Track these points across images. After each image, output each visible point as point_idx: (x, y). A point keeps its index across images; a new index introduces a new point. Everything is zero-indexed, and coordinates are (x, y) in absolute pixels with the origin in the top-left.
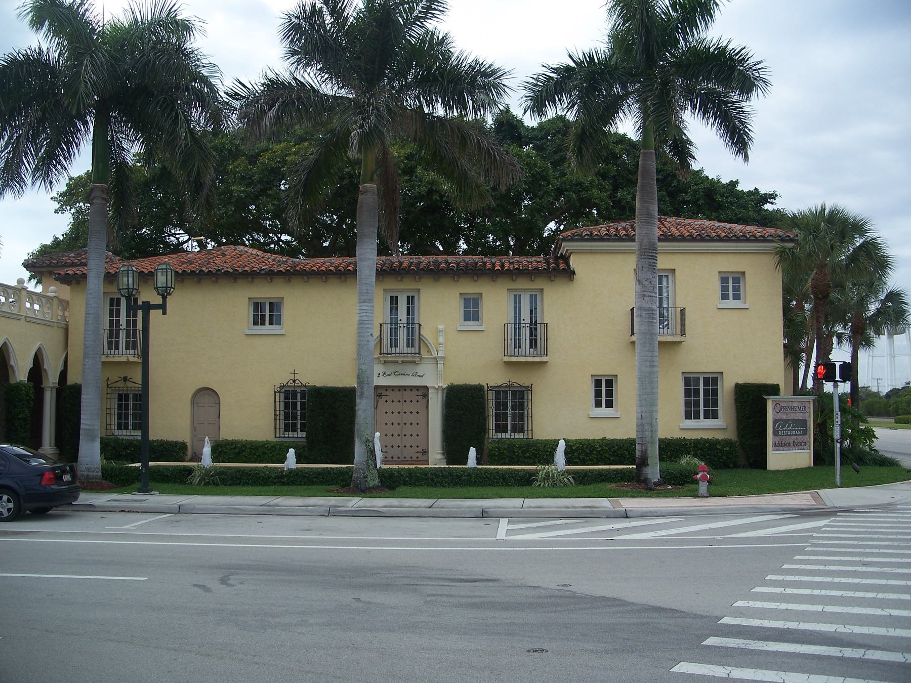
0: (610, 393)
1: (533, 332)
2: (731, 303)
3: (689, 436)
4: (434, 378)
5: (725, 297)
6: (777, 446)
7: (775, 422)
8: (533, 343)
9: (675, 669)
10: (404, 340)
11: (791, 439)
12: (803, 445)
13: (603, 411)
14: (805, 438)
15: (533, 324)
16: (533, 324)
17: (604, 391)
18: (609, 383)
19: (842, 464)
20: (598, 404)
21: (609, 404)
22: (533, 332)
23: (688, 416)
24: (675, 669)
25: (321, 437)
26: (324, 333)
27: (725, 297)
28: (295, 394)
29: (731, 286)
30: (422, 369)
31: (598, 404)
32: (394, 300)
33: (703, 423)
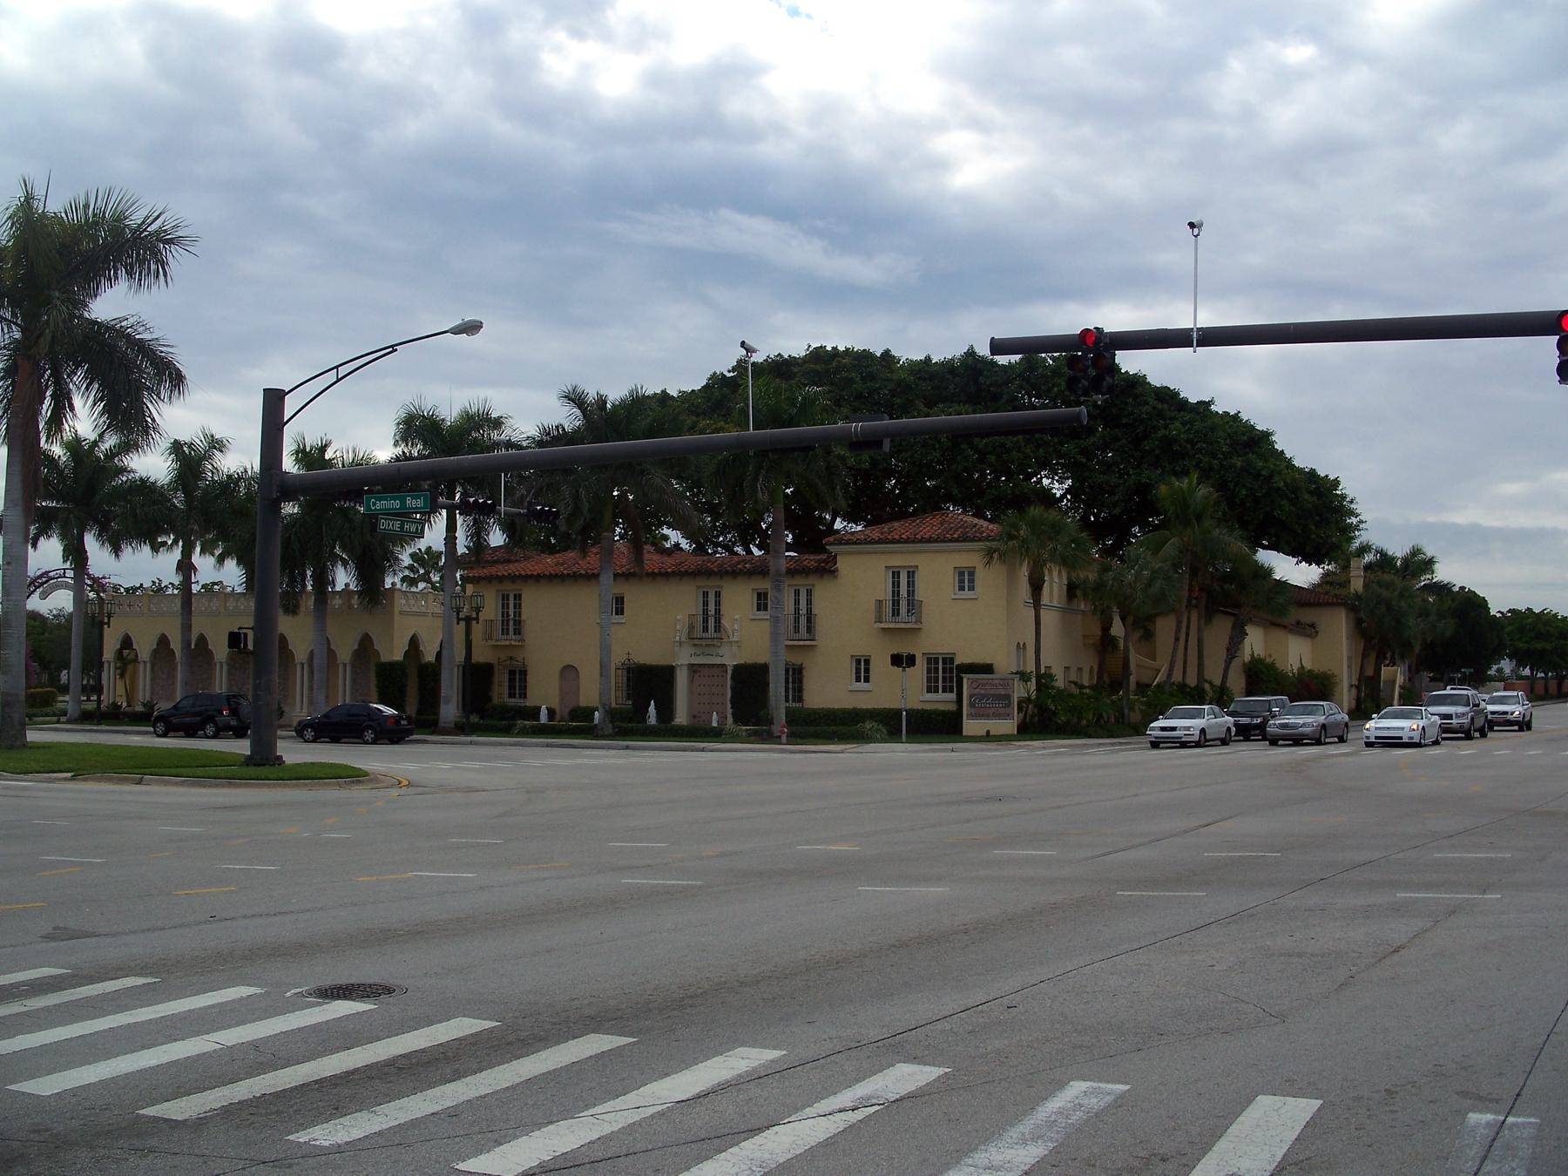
0: (867, 671)
1: (809, 620)
2: (967, 594)
3: (928, 707)
4: (730, 658)
5: (962, 588)
6: (971, 716)
7: (971, 696)
8: (810, 629)
9: (1127, 1087)
10: (709, 625)
11: (991, 711)
12: (1008, 716)
13: (862, 685)
14: (1008, 710)
15: (809, 611)
16: (809, 611)
17: (862, 668)
18: (867, 662)
19: (69, 644)
20: (858, 680)
21: (867, 680)
22: (809, 620)
23: (929, 691)
24: (1127, 1087)
25: (642, 706)
26: (657, 624)
27: (962, 588)
28: (936, 660)
29: (965, 578)
30: (724, 650)
31: (858, 680)
32: (706, 594)
33: (941, 696)
